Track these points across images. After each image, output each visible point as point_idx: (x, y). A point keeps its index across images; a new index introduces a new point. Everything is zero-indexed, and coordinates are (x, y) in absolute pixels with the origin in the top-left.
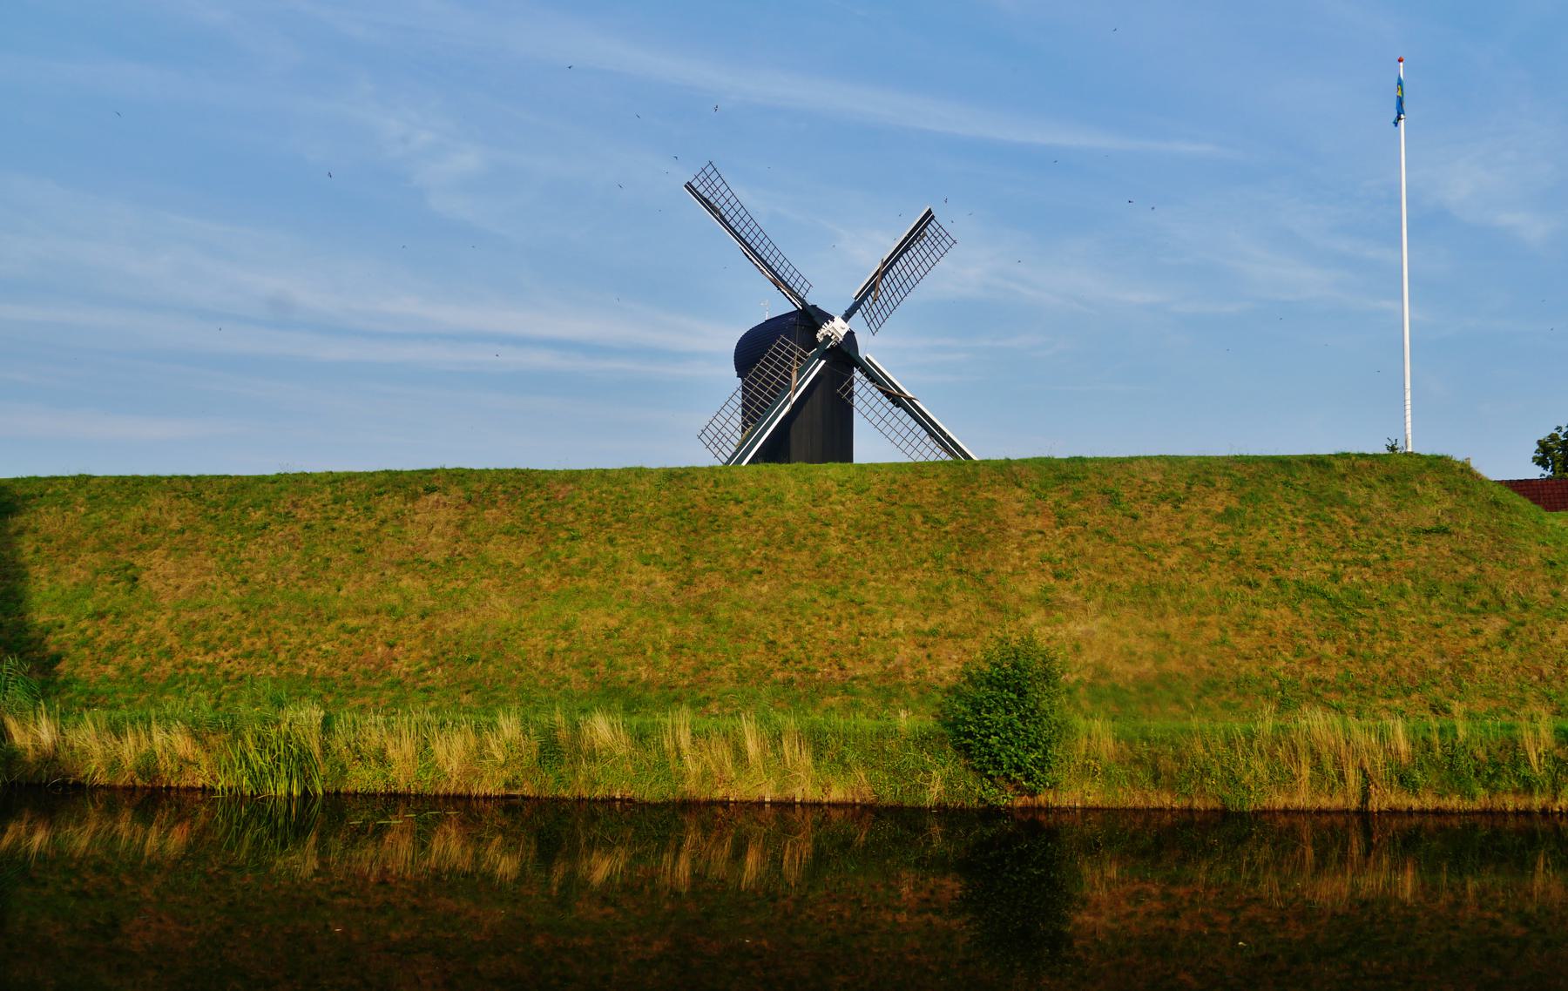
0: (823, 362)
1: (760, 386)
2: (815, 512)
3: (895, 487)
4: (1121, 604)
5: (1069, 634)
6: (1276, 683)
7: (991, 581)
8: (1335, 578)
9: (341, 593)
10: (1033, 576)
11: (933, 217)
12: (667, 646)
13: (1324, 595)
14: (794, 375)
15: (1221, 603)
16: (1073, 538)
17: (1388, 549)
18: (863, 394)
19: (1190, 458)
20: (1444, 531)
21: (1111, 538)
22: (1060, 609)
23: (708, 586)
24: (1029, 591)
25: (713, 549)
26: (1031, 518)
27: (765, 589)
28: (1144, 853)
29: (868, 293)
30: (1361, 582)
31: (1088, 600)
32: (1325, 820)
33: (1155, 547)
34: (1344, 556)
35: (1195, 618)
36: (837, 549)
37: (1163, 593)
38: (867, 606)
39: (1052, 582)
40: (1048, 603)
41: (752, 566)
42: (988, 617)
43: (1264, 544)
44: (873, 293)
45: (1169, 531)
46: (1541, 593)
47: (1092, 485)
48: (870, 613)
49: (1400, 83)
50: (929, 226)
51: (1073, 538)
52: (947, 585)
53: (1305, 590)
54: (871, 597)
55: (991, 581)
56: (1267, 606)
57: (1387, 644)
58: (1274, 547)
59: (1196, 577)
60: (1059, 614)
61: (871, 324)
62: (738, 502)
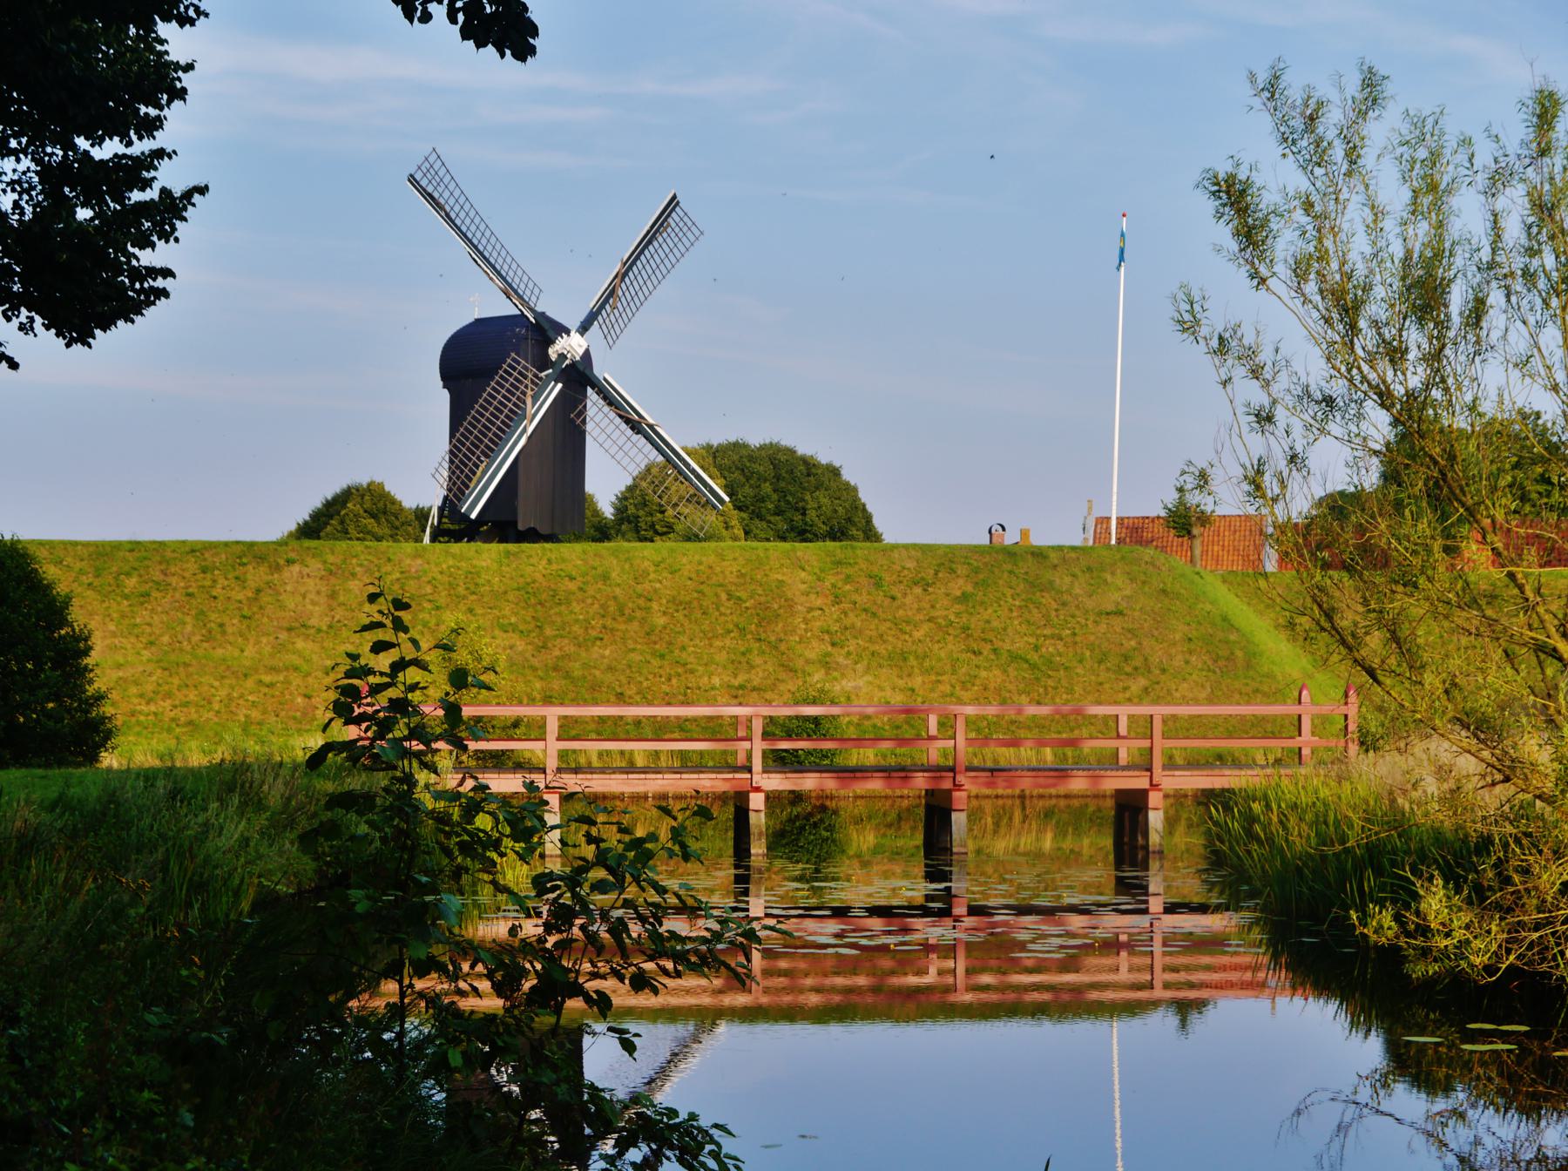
0: (560, 386)
1: (492, 414)
2: (639, 588)
3: (701, 567)
4: (880, 666)
5: (842, 689)
6: (985, 723)
7: (783, 647)
8: (1036, 648)
9: (245, 654)
10: (815, 643)
11: (678, 203)
12: (538, 697)
13: (1027, 661)
14: (529, 401)
15: (953, 666)
16: (846, 614)
17: (1077, 626)
18: (597, 417)
19: (939, 547)
20: (1120, 613)
21: (874, 615)
22: (836, 670)
23: (561, 649)
24: (812, 655)
25: (559, 620)
26: (813, 597)
27: (607, 652)
28: (890, 826)
29: (606, 301)
30: (1055, 652)
31: (856, 663)
32: (1000, 802)
33: (908, 623)
34: (1045, 632)
35: (933, 678)
36: (661, 621)
37: (911, 658)
38: (689, 666)
39: (830, 649)
40: (826, 664)
41: (594, 633)
42: (782, 675)
43: (988, 622)
44: (611, 301)
45: (919, 610)
46: (1178, 661)
47: (861, 570)
48: (692, 672)
49: (1123, 235)
50: (674, 215)
51: (846, 614)
52: (749, 651)
53: (1015, 657)
54: (691, 659)
55: (783, 647)
56: (986, 669)
57: (1064, 696)
58: (995, 624)
59: (937, 646)
60: (835, 674)
61: (609, 337)
62: (572, 578)
